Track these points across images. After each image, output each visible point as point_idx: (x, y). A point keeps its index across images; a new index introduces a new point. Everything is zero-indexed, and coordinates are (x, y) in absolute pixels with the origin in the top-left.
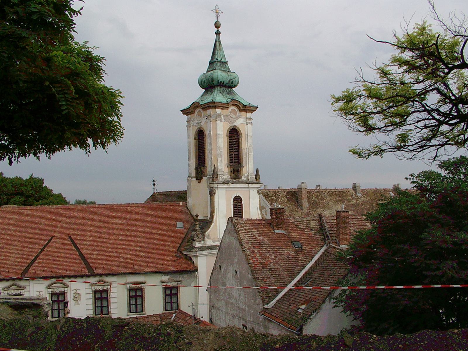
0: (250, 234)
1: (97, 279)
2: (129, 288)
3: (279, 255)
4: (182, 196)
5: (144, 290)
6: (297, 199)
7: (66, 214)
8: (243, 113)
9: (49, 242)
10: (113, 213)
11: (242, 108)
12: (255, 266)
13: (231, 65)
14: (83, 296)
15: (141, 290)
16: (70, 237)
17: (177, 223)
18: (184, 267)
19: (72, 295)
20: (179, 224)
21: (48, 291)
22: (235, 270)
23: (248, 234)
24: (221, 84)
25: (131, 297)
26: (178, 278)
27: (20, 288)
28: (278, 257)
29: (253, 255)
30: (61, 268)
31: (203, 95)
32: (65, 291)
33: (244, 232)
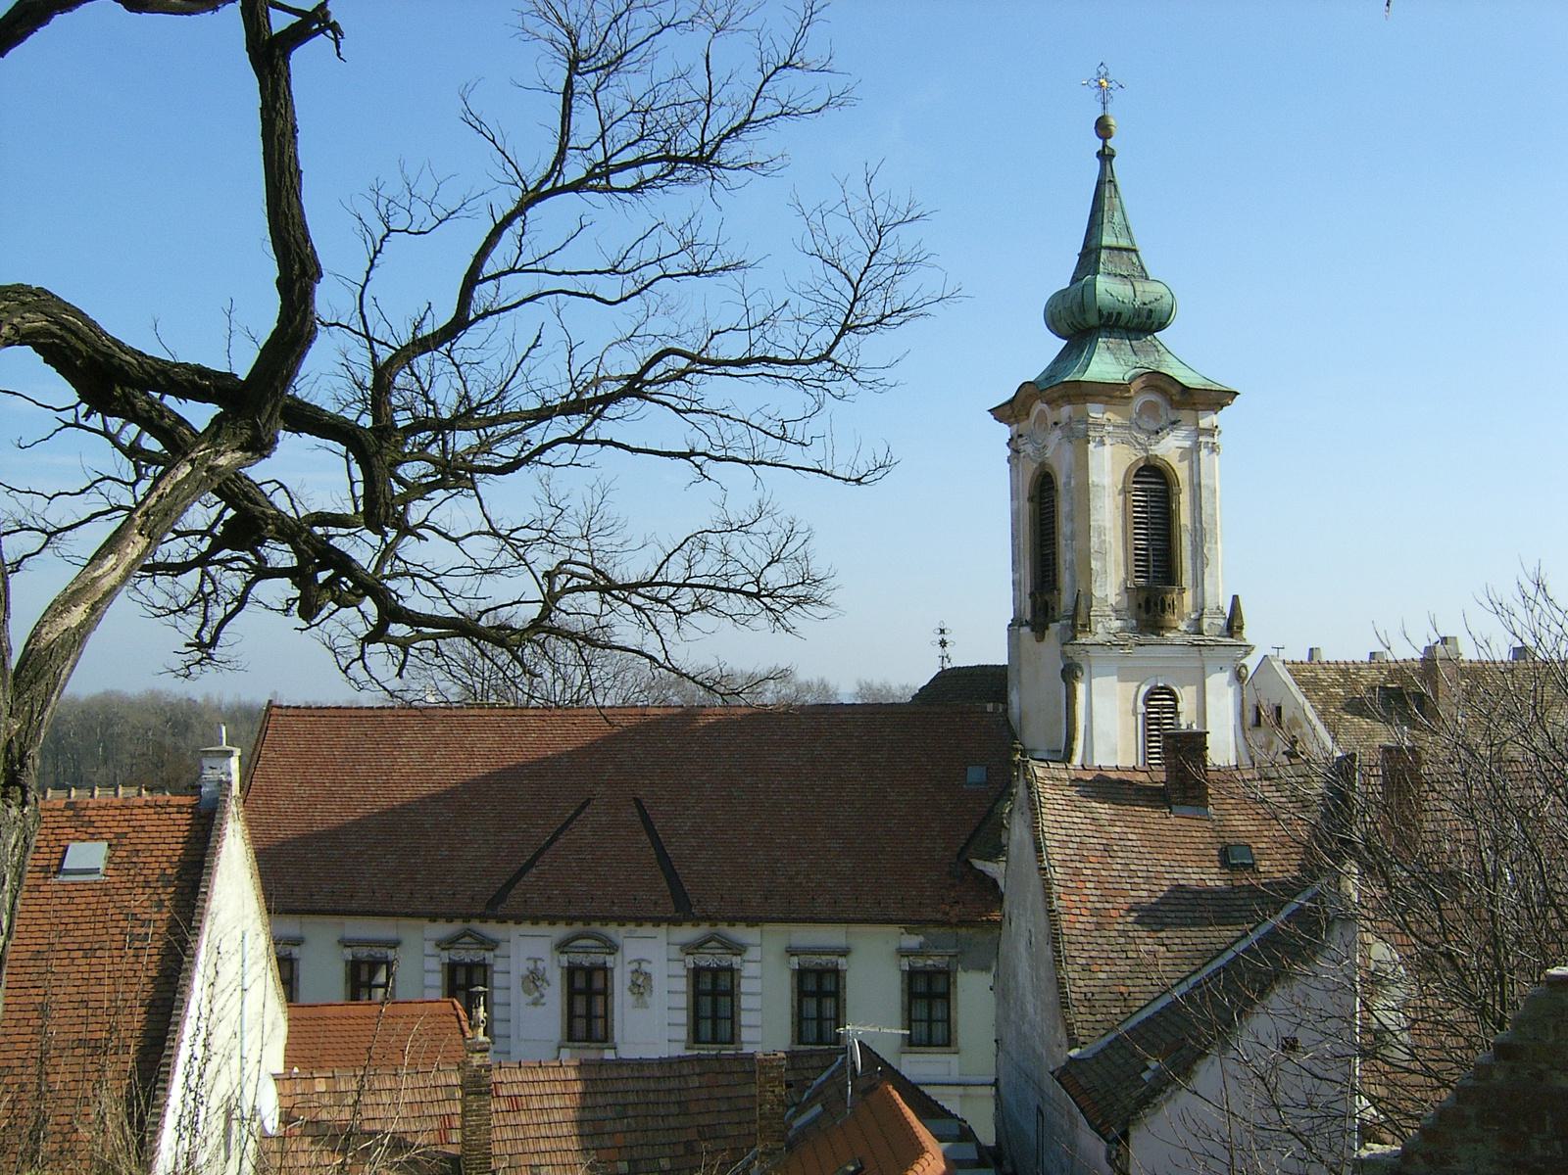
8: (1184, 415)
9: (577, 814)
11: (1176, 398)
14: (660, 983)
15: (837, 974)
16: (638, 801)
17: (969, 768)
19: (628, 977)
23: (1073, 814)
29: (1073, 885)
33: (1060, 807)
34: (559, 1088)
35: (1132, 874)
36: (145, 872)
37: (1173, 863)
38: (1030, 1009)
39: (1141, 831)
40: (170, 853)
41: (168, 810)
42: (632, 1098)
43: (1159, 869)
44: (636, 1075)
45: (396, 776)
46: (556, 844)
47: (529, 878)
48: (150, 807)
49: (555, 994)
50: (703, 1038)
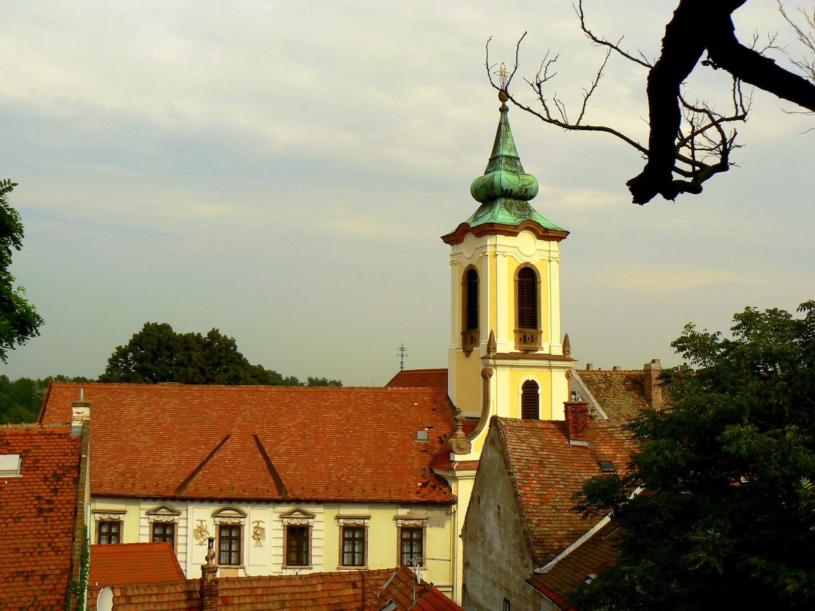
0: (526, 445)
2: (342, 525)
3: (572, 484)
4: (436, 380)
5: (368, 530)
6: (642, 388)
7: (253, 400)
10: (326, 402)
11: (541, 234)
12: (528, 499)
13: (526, 164)
19: (252, 530)
21: (215, 521)
22: (498, 505)
23: (522, 445)
24: (507, 194)
25: (344, 539)
26: (420, 513)
27: (307, 517)
28: (571, 487)
29: (526, 482)
30: (237, 485)
31: (480, 210)
32: (242, 523)
33: (515, 441)
35: (555, 476)
36: (44, 472)
37: (574, 471)
39: (556, 454)
40: (57, 461)
41: (53, 437)
42: (287, 597)
43: (568, 473)
44: (289, 584)
46: (212, 459)
47: (198, 477)
48: (42, 435)
50: (222, 562)
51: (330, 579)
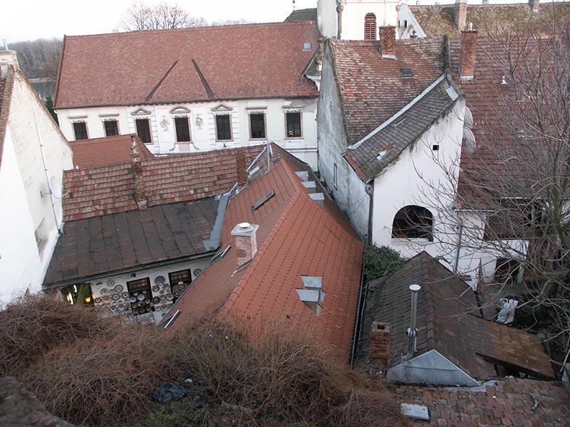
1: (218, 104)
9: (173, 66)
18: (307, 93)
20: (307, 46)
34: (168, 166)
38: (331, 129)
42: (194, 167)
45: (111, 58)
49: (172, 128)
51: (222, 153)
